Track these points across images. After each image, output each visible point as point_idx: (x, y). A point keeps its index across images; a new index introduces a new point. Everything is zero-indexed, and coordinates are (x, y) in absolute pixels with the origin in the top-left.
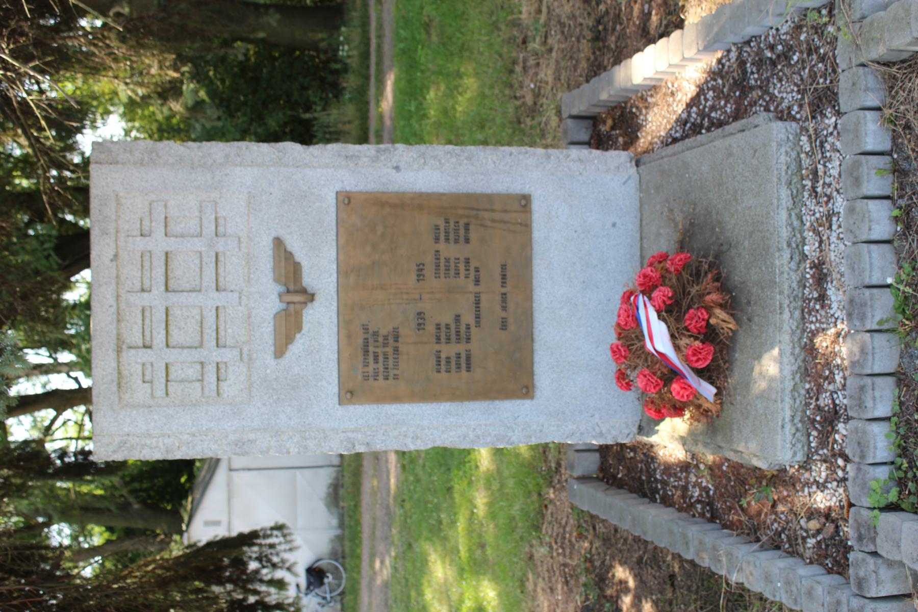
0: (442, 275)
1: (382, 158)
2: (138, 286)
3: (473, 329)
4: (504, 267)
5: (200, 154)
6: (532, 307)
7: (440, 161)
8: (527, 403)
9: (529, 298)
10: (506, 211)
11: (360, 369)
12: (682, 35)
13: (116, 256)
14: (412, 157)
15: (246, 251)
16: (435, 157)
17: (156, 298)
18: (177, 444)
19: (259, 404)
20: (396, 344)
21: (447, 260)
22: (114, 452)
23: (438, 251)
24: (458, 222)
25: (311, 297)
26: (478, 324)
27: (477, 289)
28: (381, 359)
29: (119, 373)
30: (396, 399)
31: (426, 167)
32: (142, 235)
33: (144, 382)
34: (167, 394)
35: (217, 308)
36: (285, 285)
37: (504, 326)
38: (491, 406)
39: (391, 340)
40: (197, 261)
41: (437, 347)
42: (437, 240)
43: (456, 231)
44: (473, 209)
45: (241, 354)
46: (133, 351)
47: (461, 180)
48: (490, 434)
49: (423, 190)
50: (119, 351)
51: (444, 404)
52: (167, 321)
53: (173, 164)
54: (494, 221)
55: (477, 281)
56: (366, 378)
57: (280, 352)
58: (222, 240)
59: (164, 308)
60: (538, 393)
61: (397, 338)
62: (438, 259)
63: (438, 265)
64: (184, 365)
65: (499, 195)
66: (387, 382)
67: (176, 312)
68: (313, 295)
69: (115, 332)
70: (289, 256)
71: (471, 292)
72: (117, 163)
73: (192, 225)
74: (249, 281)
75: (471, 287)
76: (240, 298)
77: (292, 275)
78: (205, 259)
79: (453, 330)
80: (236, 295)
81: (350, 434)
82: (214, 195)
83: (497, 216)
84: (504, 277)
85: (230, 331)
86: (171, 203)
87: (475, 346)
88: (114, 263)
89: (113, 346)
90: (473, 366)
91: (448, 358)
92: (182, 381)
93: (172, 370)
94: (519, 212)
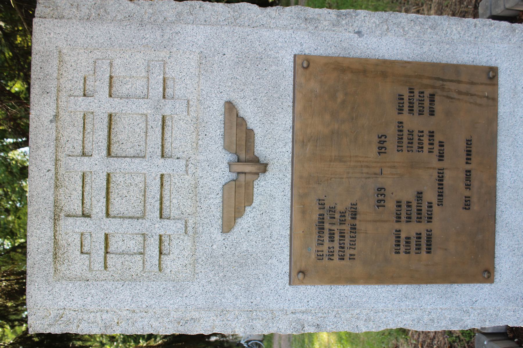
0: (405, 148)
1: (344, 22)
2: (79, 150)
3: (436, 209)
4: (469, 142)
5: (151, 11)
6: (495, 186)
7: (403, 28)
8: (486, 287)
9: (494, 177)
10: (472, 83)
11: (314, 247)
12: (491, 13)
13: (56, 116)
14: (374, 22)
15: (195, 115)
16: (398, 25)
17: (97, 164)
18: (116, 321)
19: (204, 282)
20: (353, 222)
21: (411, 133)
22: (50, 325)
23: (401, 123)
24: (423, 93)
25: (264, 168)
26: (440, 203)
27: (441, 165)
28: (337, 237)
29: (56, 243)
30: (352, 280)
31: (389, 34)
32: (85, 95)
33: (82, 253)
34: (106, 267)
35: (162, 176)
36: (236, 153)
37: (467, 206)
38: (449, 290)
39: (348, 217)
40: (143, 125)
41: (397, 226)
42: (400, 110)
43: (421, 102)
44: (438, 79)
45: (186, 227)
46: (70, 220)
47: (426, 49)
48: (445, 318)
49: (387, 57)
50: (56, 219)
51: (401, 286)
52: (108, 189)
53: (121, 20)
54: (460, 93)
55: (441, 157)
56: (320, 257)
57: (227, 227)
58: (169, 103)
59: (105, 174)
60: (497, 277)
61: (354, 215)
62: (401, 131)
63: (401, 138)
64: (125, 236)
65: (465, 66)
66: (342, 262)
67: (117, 179)
68: (266, 165)
69: (52, 198)
70: (241, 122)
71: (434, 168)
72: (63, 17)
73: (139, 85)
74: (197, 147)
75: (435, 163)
76: (187, 166)
77: (244, 143)
78: (151, 123)
79: (414, 209)
80: (183, 162)
81: (300, 316)
82: (163, 54)
83: (463, 87)
84: (469, 153)
85: (174, 201)
86: (117, 62)
87: (436, 226)
88: (54, 124)
89: (50, 214)
90: (433, 247)
91: (408, 238)
92: (122, 253)
93: (112, 241)
94: (486, 84)
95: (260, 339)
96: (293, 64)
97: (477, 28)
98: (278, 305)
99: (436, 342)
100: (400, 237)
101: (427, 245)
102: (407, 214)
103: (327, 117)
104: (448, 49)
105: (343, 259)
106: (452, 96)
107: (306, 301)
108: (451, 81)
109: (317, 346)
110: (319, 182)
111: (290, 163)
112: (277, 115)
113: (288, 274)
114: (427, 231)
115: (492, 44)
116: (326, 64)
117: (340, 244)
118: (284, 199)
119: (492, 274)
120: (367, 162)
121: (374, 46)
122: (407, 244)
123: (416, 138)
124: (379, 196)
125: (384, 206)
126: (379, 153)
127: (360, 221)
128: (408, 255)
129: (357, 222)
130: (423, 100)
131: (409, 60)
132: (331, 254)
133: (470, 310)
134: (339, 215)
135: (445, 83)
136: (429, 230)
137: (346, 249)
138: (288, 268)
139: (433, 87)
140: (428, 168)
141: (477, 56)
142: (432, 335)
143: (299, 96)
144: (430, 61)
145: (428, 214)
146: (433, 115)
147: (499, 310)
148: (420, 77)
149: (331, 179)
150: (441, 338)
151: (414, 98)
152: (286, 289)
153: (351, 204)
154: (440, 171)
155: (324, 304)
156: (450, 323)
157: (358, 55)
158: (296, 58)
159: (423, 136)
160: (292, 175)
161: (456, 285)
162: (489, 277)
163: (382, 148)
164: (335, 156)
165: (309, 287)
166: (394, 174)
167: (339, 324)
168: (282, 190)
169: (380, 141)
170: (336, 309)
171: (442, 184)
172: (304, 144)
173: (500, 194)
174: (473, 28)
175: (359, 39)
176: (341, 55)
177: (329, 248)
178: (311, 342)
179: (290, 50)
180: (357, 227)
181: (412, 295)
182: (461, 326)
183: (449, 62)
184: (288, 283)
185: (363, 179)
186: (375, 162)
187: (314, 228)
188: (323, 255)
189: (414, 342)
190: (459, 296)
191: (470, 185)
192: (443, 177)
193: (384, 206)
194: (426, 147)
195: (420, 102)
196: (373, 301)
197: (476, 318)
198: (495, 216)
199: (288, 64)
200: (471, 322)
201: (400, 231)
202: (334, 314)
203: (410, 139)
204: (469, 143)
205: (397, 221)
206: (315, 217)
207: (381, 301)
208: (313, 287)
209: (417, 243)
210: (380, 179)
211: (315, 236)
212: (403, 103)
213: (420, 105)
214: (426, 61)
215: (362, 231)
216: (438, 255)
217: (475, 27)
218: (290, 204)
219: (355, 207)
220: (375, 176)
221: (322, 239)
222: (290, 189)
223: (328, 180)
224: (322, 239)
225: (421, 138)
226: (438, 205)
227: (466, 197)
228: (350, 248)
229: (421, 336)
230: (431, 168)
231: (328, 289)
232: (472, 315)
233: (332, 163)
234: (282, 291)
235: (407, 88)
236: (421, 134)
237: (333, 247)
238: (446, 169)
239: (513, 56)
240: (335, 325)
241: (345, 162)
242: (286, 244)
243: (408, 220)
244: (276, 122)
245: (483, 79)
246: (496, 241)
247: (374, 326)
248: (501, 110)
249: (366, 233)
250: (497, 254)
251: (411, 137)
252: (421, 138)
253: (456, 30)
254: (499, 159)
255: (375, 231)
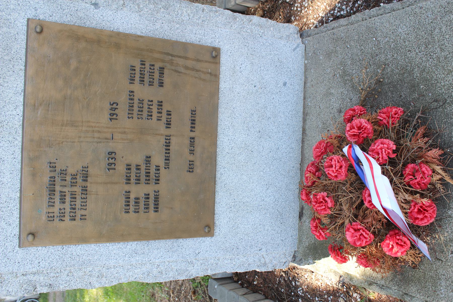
0: (135, 116)
4: (193, 112)
7: (138, 5)
8: (208, 240)
9: (214, 144)
10: (198, 60)
11: (45, 209)
20: (84, 184)
23: (132, 92)
24: (153, 65)
26: (167, 166)
27: (168, 132)
28: (68, 199)
30: (83, 240)
31: (125, 9)
37: (191, 170)
39: (79, 180)
41: (127, 188)
42: (132, 80)
43: (151, 74)
44: (168, 54)
47: (158, 26)
48: (172, 270)
49: (121, 30)
51: (131, 243)
54: (187, 68)
55: (168, 124)
56: (51, 218)
61: (85, 178)
63: (131, 106)
66: (74, 222)
71: (162, 135)
79: (143, 172)
81: (31, 277)
83: (190, 63)
84: (193, 122)
87: (163, 188)
90: (160, 207)
94: (210, 62)
95: (36, 297)
96: (26, 27)
97: (205, 12)
98: (7, 268)
99: (183, 288)
100: (129, 198)
101: (155, 204)
102: (136, 176)
103: (60, 83)
104: (178, 28)
105: (75, 220)
106: (180, 70)
107: (37, 262)
108: (180, 57)
109: (87, 299)
110: (50, 145)
111: (21, 127)
112: (7, 77)
113: (18, 236)
114: (155, 191)
115: (217, 28)
116: (60, 31)
117: (71, 205)
118: (13, 162)
119: (212, 228)
120: (98, 127)
121: (110, 19)
122: (136, 204)
123: (146, 106)
124: (110, 159)
125: (115, 169)
126: (111, 119)
127: (91, 183)
128: (137, 214)
129: (88, 184)
130: (154, 73)
131: (142, 34)
132: (62, 215)
133: (194, 261)
134: (71, 177)
135: (174, 58)
136: (156, 191)
137: (77, 210)
138: (18, 230)
139: (163, 61)
140: (156, 134)
141: (203, 37)
142: (180, 283)
143: (30, 60)
144: (161, 37)
145: (155, 176)
146: (162, 86)
147: (219, 260)
148: (151, 51)
149: (62, 143)
150: (187, 285)
151: (145, 69)
152: (15, 251)
153: (83, 167)
154: (167, 138)
155: (55, 263)
156: (177, 274)
157: (93, 25)
158: (30, 23)
159: (152, 105)
160: (23, 138)
161: (181, 239)
162: (209, 231)
163: (114, 114)
164: (67, 121)
165: (40, 248)
166: (125, 140)
167: (72, 282)
168: (12, 153)
169: (112, 108)
170: (68, 268)
171: (169, 150)
172: (35, 108)
173: (220, 159)
174: (201, 12)
175: (95, 11)
176: (76, 24)
177: (60, 209)
178: (82, 296)
179: (24, 14)
180: (88, 189)
181: (142, 251)
182: (186, 276)
183: (178, 40)
184: (18, 246)
185: (94, 144)
186: (107, 128)
187: (45, 190)
188: (54, 217)
189: (167, 289)
190: (184, 249)
191: (194, 151)
192: (169, 143)
193: (115, 169)
194: (155, 115)
195: (151, 74)
196: (105, 258)
197: (199, 267)
198: (215, 177)
199: (21, 28)
200: (197, 271)
201: (129, 192)
202: (66, 273)
203: (141, 107)
204: (194, 113)
205: (127, 183)
206: (46, 179)
207: (112, 257)
208: (44, 248)
209: (146, 203)
210: (111, 144)
211: (46, 198)
212: (135, 74)
213: (150, 77)
214: (157, 37)
215: (93, 193)
216: (164, 213)
217: (203, 11)
218: (20, 167)
219: (86, 169)
220: (107, 140)
221: (53, 201)
222: (20, 152)
223: (59, 144)
224: (53, 201)
225: (151, 107)
226: (165, 168)
227: (190, 161)
228: (81, 209)
229: (172, 284)
230: (159, 134)
231: (60, 249)
232: (196, 265)
233: (64, 128)
234: (11, 254)
235: (139, 60)
236: (151, 103)
237: (64, 209)
238: (173, 135)
239: (233, 40)
240: (68, 283)
241: (77, 126)
242: (16, 207)
243: (137, 182)
244: (6, 85)
245: (207, 57)
246: (216, 200)
247: (107, 282)
248: (224, 84)
249: (97, 194)
250: (217, 211)
251: (141, 105)
252: (151, 107)
253: (186, 12)
254: (219, 129)
255: (104, 192)
